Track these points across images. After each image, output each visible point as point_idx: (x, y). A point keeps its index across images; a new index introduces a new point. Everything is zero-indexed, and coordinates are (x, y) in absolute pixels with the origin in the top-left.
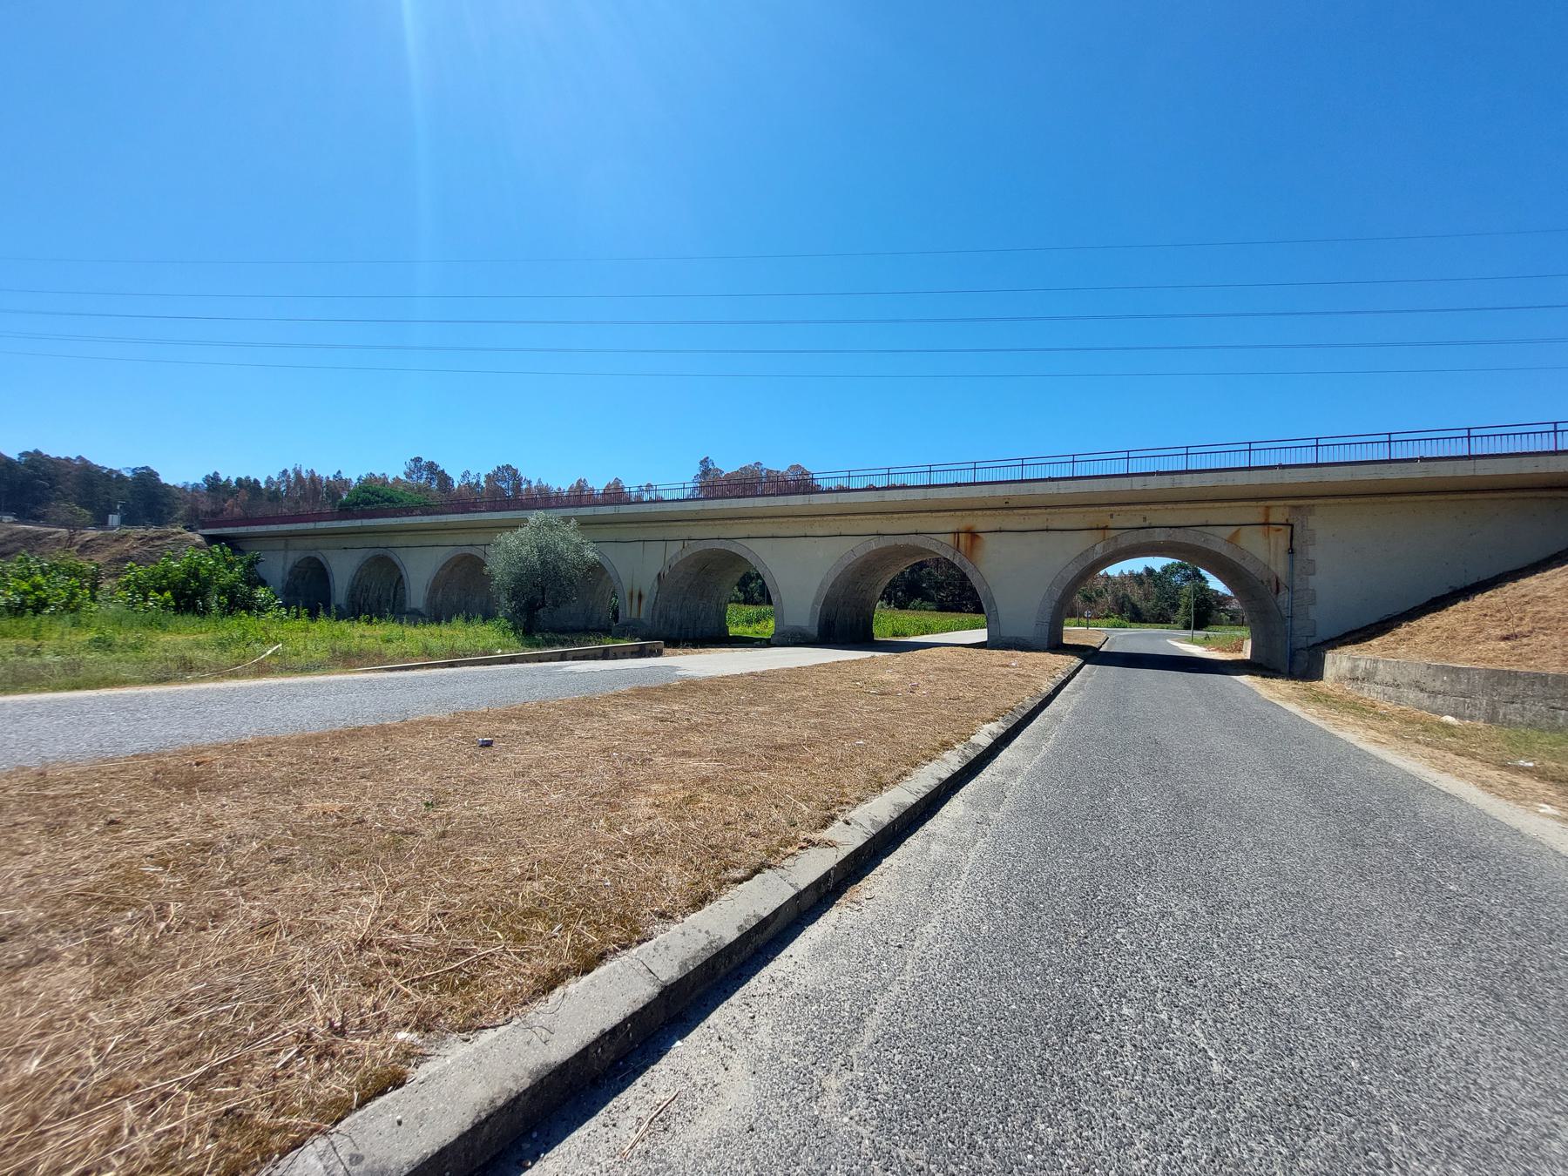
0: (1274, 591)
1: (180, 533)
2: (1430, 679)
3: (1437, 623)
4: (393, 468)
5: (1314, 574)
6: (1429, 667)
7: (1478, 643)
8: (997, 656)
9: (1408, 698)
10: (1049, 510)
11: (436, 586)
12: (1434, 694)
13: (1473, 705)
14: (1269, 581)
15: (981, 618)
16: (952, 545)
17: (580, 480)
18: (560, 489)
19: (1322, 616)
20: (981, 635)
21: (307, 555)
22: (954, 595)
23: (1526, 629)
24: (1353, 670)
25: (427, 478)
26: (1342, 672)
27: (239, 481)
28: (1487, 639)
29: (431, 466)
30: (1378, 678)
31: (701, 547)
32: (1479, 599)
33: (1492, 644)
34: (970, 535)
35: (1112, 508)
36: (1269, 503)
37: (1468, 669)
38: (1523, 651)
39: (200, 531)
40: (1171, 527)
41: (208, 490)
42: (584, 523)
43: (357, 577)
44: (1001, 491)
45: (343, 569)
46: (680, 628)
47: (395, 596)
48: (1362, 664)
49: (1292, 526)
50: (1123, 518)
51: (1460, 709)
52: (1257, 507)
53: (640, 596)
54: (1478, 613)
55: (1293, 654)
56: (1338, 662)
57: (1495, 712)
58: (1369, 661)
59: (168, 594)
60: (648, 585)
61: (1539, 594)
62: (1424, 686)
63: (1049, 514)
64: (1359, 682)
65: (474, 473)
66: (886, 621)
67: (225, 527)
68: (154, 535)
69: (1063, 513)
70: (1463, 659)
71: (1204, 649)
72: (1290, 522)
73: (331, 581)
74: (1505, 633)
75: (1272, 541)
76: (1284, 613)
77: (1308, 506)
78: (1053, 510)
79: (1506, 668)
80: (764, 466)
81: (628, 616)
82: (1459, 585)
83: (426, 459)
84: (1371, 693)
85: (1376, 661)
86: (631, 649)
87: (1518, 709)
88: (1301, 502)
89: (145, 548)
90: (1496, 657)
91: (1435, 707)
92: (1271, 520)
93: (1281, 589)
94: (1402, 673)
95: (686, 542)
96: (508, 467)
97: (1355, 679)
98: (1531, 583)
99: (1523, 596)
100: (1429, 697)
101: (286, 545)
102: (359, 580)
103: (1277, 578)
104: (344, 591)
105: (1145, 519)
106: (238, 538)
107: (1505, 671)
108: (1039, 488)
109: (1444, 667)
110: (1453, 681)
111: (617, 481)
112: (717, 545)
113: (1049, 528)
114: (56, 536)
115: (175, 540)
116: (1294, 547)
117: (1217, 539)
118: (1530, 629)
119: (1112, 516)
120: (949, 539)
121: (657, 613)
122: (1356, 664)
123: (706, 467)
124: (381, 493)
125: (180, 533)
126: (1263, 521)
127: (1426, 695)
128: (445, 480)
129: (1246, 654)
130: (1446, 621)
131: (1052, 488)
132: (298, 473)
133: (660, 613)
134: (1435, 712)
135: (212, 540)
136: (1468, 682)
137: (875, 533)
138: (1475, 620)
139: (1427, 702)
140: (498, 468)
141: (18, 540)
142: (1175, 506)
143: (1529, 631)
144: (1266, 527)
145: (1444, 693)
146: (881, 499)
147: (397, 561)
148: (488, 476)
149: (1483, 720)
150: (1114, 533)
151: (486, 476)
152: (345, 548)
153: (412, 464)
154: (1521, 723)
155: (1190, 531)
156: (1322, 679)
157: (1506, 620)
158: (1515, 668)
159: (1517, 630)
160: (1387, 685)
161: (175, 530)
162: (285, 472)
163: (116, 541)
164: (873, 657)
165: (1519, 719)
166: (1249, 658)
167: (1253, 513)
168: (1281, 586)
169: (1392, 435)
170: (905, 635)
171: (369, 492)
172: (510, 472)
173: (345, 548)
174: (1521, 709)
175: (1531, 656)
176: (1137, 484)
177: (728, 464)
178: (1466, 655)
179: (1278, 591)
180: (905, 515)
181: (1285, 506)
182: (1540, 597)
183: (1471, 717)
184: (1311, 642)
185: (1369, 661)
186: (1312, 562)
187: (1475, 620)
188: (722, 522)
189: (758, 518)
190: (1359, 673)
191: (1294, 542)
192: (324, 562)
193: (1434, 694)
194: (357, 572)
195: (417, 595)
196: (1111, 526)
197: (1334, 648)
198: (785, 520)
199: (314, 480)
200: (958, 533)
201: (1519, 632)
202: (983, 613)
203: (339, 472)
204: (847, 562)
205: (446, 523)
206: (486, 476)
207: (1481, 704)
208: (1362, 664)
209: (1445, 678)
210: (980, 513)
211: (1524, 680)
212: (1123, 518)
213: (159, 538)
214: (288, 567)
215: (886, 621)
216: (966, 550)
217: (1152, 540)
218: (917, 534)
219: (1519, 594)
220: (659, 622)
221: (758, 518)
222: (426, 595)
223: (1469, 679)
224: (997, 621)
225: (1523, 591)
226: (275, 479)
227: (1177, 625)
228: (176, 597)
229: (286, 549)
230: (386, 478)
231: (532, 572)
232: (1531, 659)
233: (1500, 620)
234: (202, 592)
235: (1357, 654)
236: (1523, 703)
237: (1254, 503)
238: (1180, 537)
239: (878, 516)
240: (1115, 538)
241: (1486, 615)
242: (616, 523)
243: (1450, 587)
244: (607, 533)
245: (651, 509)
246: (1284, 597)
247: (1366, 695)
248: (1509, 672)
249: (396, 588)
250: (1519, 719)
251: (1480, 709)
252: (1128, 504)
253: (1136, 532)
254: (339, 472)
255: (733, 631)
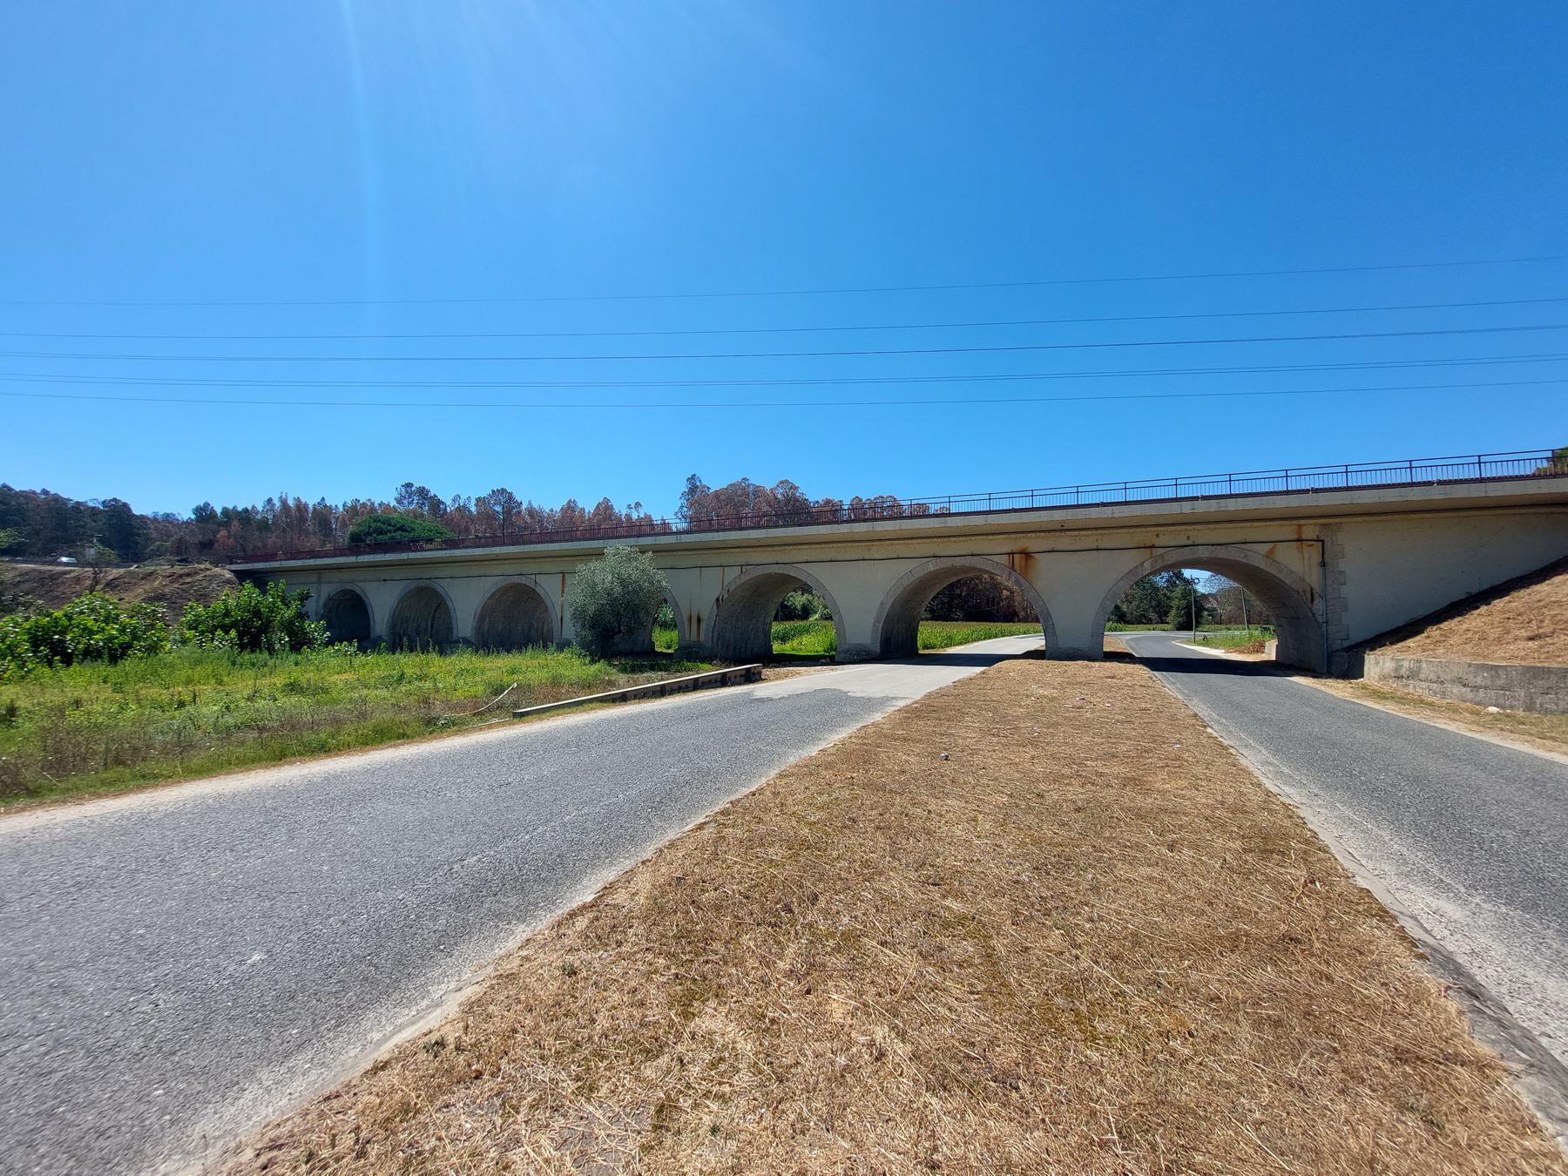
0: (1309, 599)
1: (208, 569)
2: (1471, 676)
3: (1465, 626)
4: (382, 493)
5: (1345, 584)
6: (1470, 665)
7: (1508, 643)
8: (1054, 669)
9: (1452, 693)
10: (1099, 532)
11: (485, 615)
12: (1476, 688)
13: (1512, 697)
14: (1304, 591)
15: (1039, 627)
16: (1007, 564)
17: (570, 500)
18: (552, 510)
19: (1355, 625)
20: (1037, 642)
21: (343, 588)
22: (943, 603)
23: (1548, 630)
24: (1397, 669)
25: (418, 503)
26: (1386, 671)
27: (225, 511)
28: (1516, 640)
29: (422, 492)
30: (1422, 676)
31: (760, 571)
32: (1498, 604)
33: (1522, 644)
34: (1023, 556)
35: (1159, 529)
36: (1302, 522)
37: (1506, 666)
38: (1550, 649)
39: (228, 566)
40: (1213, 545)
41: (197, 521)
42: (658, 550)
43: (399, 608)
44: (1058, 516)
45: (383, 603)
46: (735, 649)
47: (432, 626)
48: (1406, 664)
49: (1323, 541)
50: (1168, 537)
51: (1501, 701)
52: (1290, 525)
53: (699, 620)
54: (1502, 616)
55: (1330, 655)
56: (1381, 662)
57: (1533, 703)
58: (1412, 662)
59: (233, 633)
60: (706, 607)
61: (1552, 599)
62: (1467, 682)
63: (1099, 535)
64: (1404, 680)
65: (464, 497)
66: (929, 632)
67: (255, 562)
68: (182, 572)
69: (1112, 534)
70: (1499, 657)
71: (1223, 651)
72: (1321, 538)
73: (370, 611)
74: (1529, 634)
75: (1306, 556)
76: (1320, 620)
77: (1337, 523)
78: (1103, 532)
79: (1539, 665)
80: (750, 482)
81: (687, 638)
82: (1475, 590)
83: (417, 485)
84: (1417, 689)
85: (1419, 661)
86: (740, 673)
87: (1552, 699)
88: (1331, 521)
89: (176, 586)
90: (1527, 655)
91: (1477, 699)
92: (1304, 537)
93: (1315, 598)
94: (1445, 671)
95: (744, 567)
96: (503, 491)
97: (1400, 677)
98: (1543, 589)
99: (1540, 601)
100: (1471, 691)
101: (319, 578)
102: (400, 612)
103: (1311, 589)
104: (385, 621)
105: (1188, 538)
106: (267, 572)
107: (1539, 667)
108: (1095, 513)
109: (1483, 665)
110: (1493, 677)
111: (606, 500)
112: (775, 570)
113: (1100, 547)
114: (72, 575)
115: (205, 576)
116: (1326, 561)
117: (1256, 555)
118: (1552, 630)
119: (1157, 535)
120: (1004, 560)
121: (716, 634)
122: (1400, 664)
123: (694, 488)
124: (393, 523)
125: (208, 569)
126: (1296, 537)
127: (1469, 689)
128: (436, 504)
129: (1270, 653)
130: (1474, 624)
131: (1107, 512)
132: (284, 502)
133: (719, 634)
134: (1478, 704)
135: (242, 576)
136: (1507, 677)
137: (931, 554)
138: (1500, 622)
139: (1470, 696)
140: (493, 491)
141: (33, 580)
142: (1216, 526)
143: (1551, 632)
144: (1299, 543)
145: (1486, 688)
146: (943, 525)
147: (442, 592)
148: (478, 500)
149: (1521, 709)
150: (1161, 551)
151: (476, 499)
152: (385, 580)
153: (403, 490)
154: (1556, 711)
155: (1230, 548)
156: (1362, 677)
157: (1528, 623)
158: (1546, 665)
159: (1540, 631)
160: (1431, 681)
161: (202, 566)
162: (270, 501)
163: (143, 579)
164: (983, 673)
165: (1555, 707)
166: (1274, 659)
167: (1288, 531)
168: (1316, 596)
169: (1413, 462)
170: (933, 648)
171: (380, 521)
172: (506, 498)
173: (385, 580)
174: (1556, 699)
175: (1558, 654)
176: (1186, 507)
177: (716, 481)
178: (1500, 653)
179: (1312, 600)
180: (961, 539)
181: (1316, 524)
182: (1555, 602)
183: (1511, 707)
184: (1346, 644)
185: (1412, 662)
186: (1342, 573)
187: (1500, 622)
188: (779, 548)
189: (818, 543)
190: (1403, 672)
191: (1326, 556)
192: (362, 595)
193: (1476, 688)
194: (398, 604)
195: (465, 620)
196: (1157, 544)
197: (1372, 649)
198: (844, 545)
199: (301, 507)
200: (1013, 554)
201: (1542, 633)
202: (1039, 622)
203: (323, 499)
204: (906, 583)
205: (498, 555)
206: (476, 499)
207: (1519, 696)
208: (1406, 664)
209: (1485, 675)
210: (1033, 535)
211: (1556, 674)
212: (1168, 537)
213: (188, 575)
214: (322, 602)
215: (929, 632)
216: (1021, 568)
217: (1196, 556)
218: (972, 555)
219: (1535, 599)
220: (717, 643)
221: (818, 543)
222: (475, 624)
223: (1507, 675)
224: (1054, 634)
225: (1538, 597)
226: (260, 509)
227: (1170, 626)
228: (240, 636)
229: (319, 582)
230: (373, 504)
231: (613, 602)
232: (1559, 657)
233: (1522, 623)
234: (266, 628)
235: (1400, 656)
236: (1556, 694)
237: (1288, 522)
238: (1222, 553)
239: (935, 540)
240: (1162, 555)
241: (1509, 618)
242: (674, 551)
243: (1467, 593)
244: (668, 560)
245: (730, 535)
246: (1319, 605)
247: (1411, 691)
248: (1543, 668)
249: (433, 617)
250: (1555, 707)
251: (1519, 700)
252: (1173, 525)
253: (1181, 550)
254: (323, 499)
255: (777, 647)
